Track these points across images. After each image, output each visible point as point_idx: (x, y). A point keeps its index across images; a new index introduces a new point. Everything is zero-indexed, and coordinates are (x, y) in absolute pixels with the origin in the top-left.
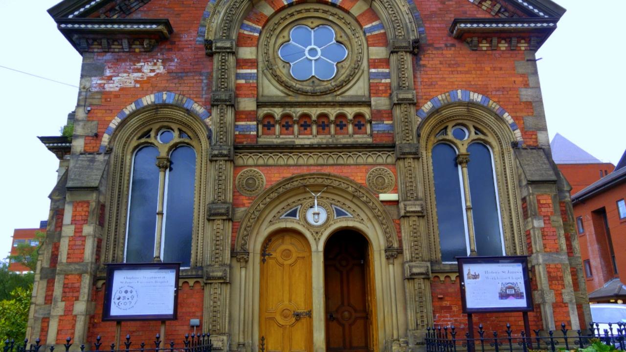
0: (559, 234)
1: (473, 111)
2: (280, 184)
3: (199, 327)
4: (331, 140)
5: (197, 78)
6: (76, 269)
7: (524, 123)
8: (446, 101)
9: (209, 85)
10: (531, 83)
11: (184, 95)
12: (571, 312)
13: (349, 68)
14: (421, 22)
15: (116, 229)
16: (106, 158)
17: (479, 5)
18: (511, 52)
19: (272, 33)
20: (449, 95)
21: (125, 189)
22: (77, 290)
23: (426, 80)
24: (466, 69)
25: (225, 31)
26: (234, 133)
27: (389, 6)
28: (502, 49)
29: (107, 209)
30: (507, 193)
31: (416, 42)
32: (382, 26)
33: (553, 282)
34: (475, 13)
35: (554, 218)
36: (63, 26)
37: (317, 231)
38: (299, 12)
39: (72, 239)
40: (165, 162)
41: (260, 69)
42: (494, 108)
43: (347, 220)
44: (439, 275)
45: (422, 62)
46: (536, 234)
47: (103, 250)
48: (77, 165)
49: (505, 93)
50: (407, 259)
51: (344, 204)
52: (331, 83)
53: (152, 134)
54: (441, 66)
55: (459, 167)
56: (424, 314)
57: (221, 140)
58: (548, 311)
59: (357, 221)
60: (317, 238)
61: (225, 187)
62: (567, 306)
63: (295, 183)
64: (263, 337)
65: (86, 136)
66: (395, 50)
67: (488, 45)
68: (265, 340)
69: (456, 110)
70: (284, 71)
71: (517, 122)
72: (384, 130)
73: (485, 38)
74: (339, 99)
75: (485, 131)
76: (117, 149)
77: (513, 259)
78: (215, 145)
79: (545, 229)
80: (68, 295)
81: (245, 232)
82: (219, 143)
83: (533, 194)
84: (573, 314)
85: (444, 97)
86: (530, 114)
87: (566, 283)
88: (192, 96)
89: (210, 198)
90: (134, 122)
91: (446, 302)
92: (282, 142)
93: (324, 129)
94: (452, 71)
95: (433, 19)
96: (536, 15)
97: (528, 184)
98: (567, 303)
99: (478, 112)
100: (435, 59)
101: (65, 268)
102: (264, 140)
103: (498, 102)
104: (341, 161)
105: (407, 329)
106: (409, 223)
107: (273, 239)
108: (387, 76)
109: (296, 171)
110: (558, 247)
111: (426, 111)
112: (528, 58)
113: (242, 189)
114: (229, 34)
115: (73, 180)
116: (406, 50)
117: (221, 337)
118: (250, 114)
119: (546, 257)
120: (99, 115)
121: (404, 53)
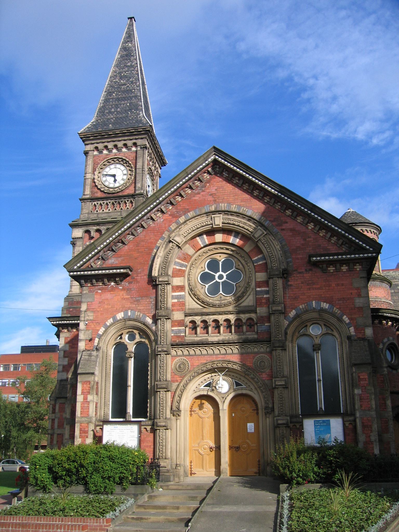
0: (371, 398)
5: (148, 300)
6: (86, 421)
10: (363, 294)
12: (375, 447)
17: (329, 240)
20: (307, 305)
22: (86, 432)
23: (292, 295)
24: (318, 286)
29: (99, 385)
32: (264, 258)
33: (365, 429)
34: (326, 245)
35: (369, 388)
36: (72, 273)
39: (83, 403)
42: (337, 312)
43: (242, 389)
44: (296, 424)
45: (290, 283)
54: (302, 285)
59: (248, 390)
62: (373, 444)
66: (271, 277)
67: (334, 268)
71: (352, 321)
73: (332, 264)
79: (362, 396)
80: (82, 434)
85: (304, 307)
88: (145, 313)
94: (309, 288)
95: (298, 252)
96: (364, 249)
98: (373, 442)
99: (326, 316)
101: (80, 419)
103: (339, 309)
108: (267, 292)
109: (209, 359)
116: (278, 276)
120: (93, 326)
121: (277, 279)
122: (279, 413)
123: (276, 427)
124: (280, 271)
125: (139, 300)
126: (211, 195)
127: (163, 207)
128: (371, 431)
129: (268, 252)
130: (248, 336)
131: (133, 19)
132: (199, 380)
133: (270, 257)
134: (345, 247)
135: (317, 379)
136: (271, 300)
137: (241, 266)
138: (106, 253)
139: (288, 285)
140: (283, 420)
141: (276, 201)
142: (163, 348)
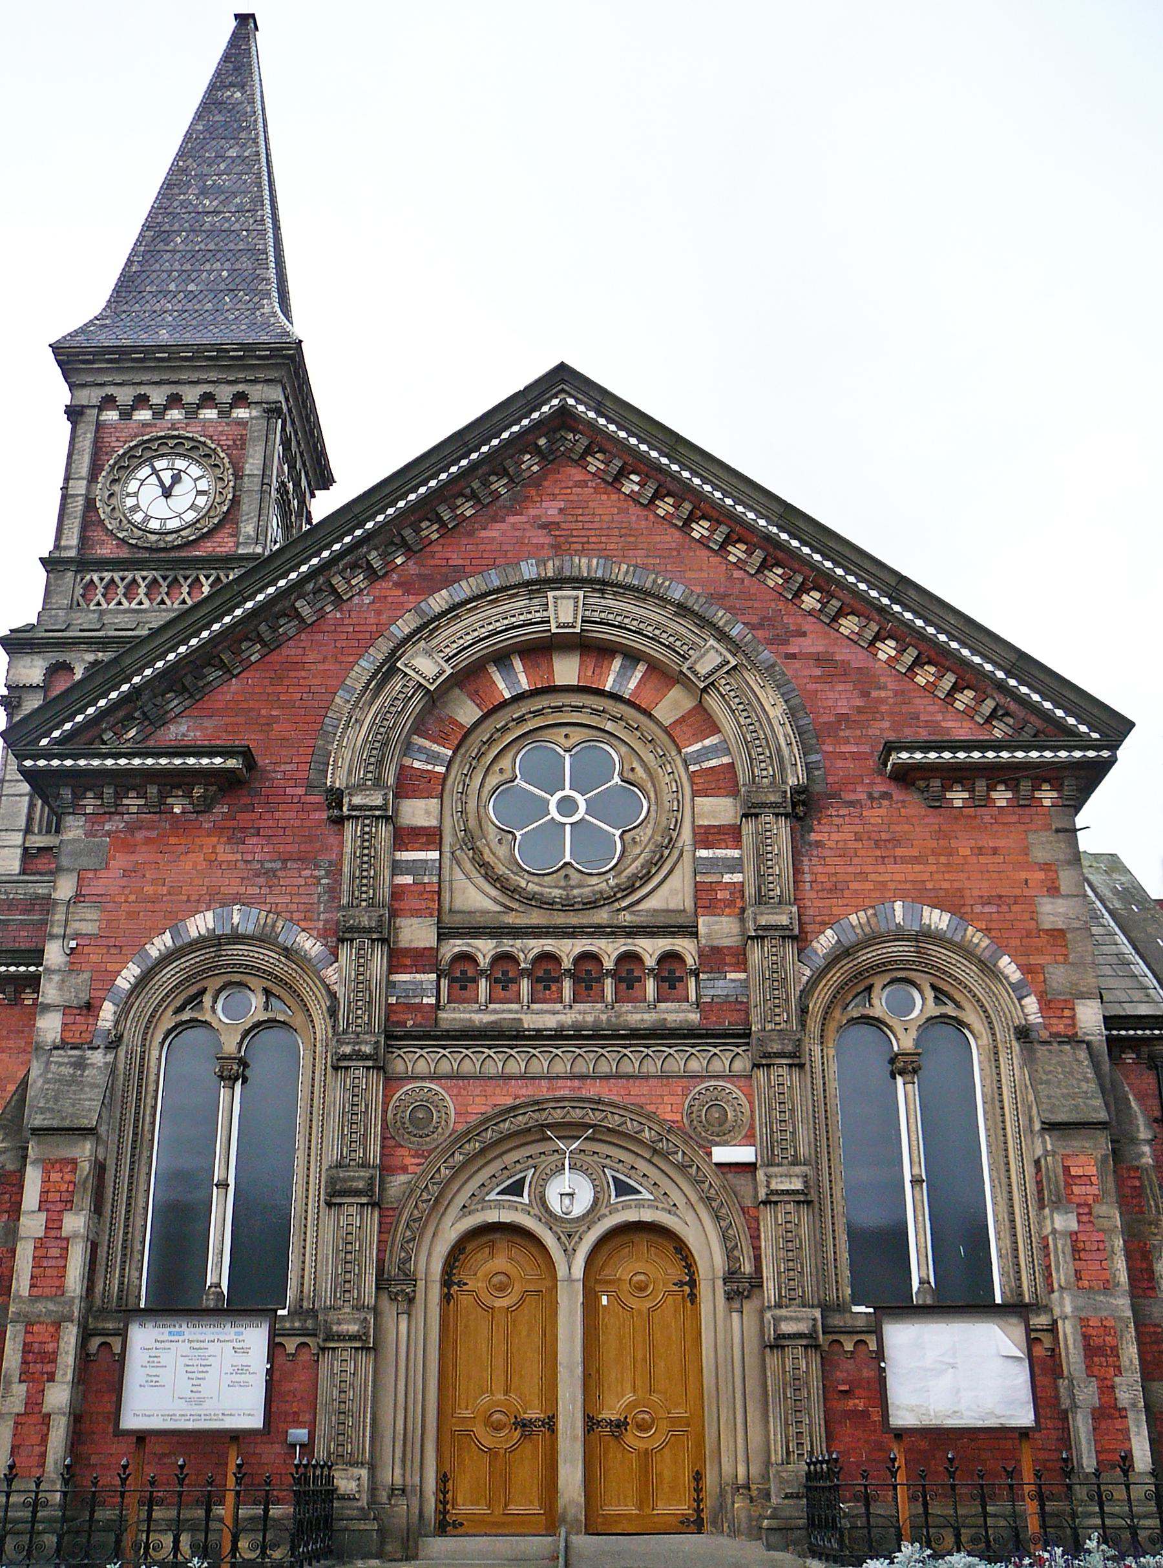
0: (1113, 1246)
1: (929, 952)
2: (486, 1121)
3: (308, 1447)
4: (604, 1017)
5: (307, 873)
6: (49, 1312)
7: (1044, 981)
8: (867, 929)
9: (333, 892)
11: (278, 914)
13: (650, 845)
14: (814, 741)
15: (127, 1219)
16: (110, 1058)
17: (949, 700)
18: (1019, 811)
19: (474, 763)
20: (875, 915)
21: (147, 1127)
22: (51, 1358)
23: (821, 878)
25: (371, 768)
26: (387, 1000)
27: (741, 707)
28: (999, 803)
30: (1003, 1146)
31: (798, 790)
33: (1096, 1359)
34: (939, 717)
35: (1101, 1210)
36: (28, 763)
37: (569, 1228)
38: (538, 713)
39: (40, 1244)
40: (235, 1067)
41: (446, 849)
42: (978, 944)
43: (640, 1205)
44: (842, 1338)
45: (813, 837)
46: (1059, 1246)
47: (100, 1269)
48: (50, 1076)
49: (1005, 908)
50: (769, 1301)
51: (633, 1167)
52: (607, 881)
53: (207, 999)
55: (900, 1080)
56: (805, 1429)
57: (359, 1021)
58: (1082, 1426)
59: (663, 1209)
60: (570, 1248)
61: (366, 1130)
62: (1126, 1417)
63: (520, 1118)
64: (445, 1475)
65: (66, 1007)
66: (753, 811)
68: (451, 1482)
69: (879, 952)
70: (502, 851)
72: (727, 996)
73: (959, 781)
74: (626, 918)
75: (958, 997)
76: (132, 1036)
77: (1016, 1309)
78: (345, 1032)
79: (1081, 1237)
80: (33, 1368)
81: (408, 1233)
82: (352, 1028)
83: (1054, 1153)
84: (1138, 1434)
85: (863, 920)
86: (1061, 959)
87: (1125, 1362)
89: (332, 1155)
90: (169, 975)
91: (857, 1401)
92: (492, 1022)
93: (589, 988)
95: (842, 734)
96: (1071, 732)
97: (1043, 1129)
98: (1125, 1409)
100: (846, 828)
101: (25, 1308)
102: (454, 1016)
103: (987, 931)
104: (627, 1068)
105: (768, 1463)
106: (776, 1218)
107: (470, 1247)
108: (735, 866)
109: (523, 1092)
110: (1108, 1277)
111: (821, 952)
112: (1060, 826)
113: (401, 1131)
114: (380, 774)
115: (42, 1111)
116: (777, 811)
117: (356, 1471)
118: (422, 955)
119: (1081, 1302)
120: (94, 958)
122: (780, 1296)
123: (771, 1347)
124: (785, 792)
125: (274, 871)
126: (544, 526)
127: (374, 553)
128: (1119, 1371)
129: (741, 726)
130: (666, 1016)
131: (251, 21)
132: (483, 1171)
133: (747, 742)
134: (1001, 726)
135: (907, 1178)
136: (750, 891)
137: (640, 771)
138: (158, 701)
139: (810, 844)
140: (798, 1319)
141: (771, 561)
142: (358, 1043)
